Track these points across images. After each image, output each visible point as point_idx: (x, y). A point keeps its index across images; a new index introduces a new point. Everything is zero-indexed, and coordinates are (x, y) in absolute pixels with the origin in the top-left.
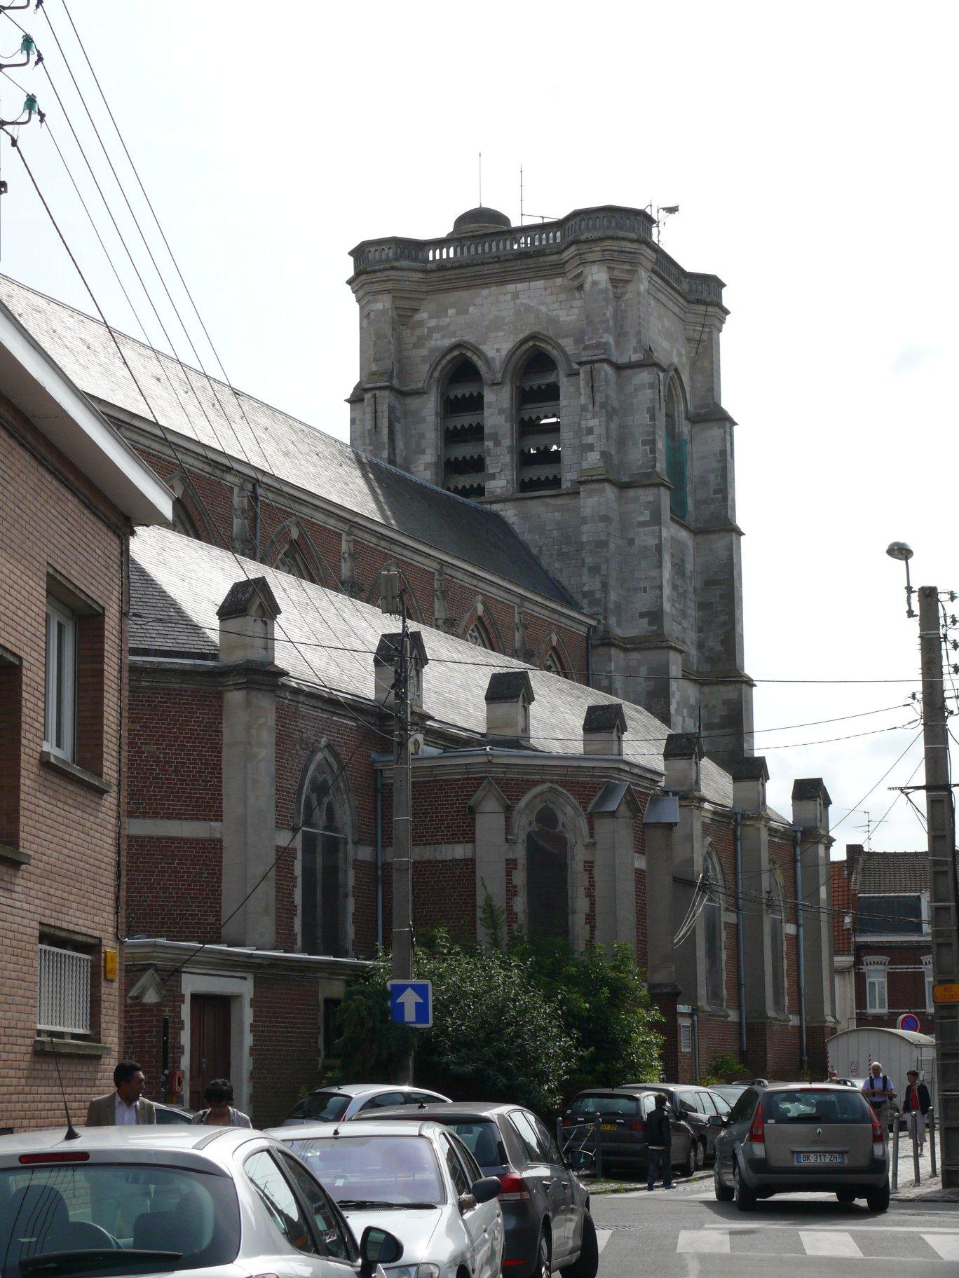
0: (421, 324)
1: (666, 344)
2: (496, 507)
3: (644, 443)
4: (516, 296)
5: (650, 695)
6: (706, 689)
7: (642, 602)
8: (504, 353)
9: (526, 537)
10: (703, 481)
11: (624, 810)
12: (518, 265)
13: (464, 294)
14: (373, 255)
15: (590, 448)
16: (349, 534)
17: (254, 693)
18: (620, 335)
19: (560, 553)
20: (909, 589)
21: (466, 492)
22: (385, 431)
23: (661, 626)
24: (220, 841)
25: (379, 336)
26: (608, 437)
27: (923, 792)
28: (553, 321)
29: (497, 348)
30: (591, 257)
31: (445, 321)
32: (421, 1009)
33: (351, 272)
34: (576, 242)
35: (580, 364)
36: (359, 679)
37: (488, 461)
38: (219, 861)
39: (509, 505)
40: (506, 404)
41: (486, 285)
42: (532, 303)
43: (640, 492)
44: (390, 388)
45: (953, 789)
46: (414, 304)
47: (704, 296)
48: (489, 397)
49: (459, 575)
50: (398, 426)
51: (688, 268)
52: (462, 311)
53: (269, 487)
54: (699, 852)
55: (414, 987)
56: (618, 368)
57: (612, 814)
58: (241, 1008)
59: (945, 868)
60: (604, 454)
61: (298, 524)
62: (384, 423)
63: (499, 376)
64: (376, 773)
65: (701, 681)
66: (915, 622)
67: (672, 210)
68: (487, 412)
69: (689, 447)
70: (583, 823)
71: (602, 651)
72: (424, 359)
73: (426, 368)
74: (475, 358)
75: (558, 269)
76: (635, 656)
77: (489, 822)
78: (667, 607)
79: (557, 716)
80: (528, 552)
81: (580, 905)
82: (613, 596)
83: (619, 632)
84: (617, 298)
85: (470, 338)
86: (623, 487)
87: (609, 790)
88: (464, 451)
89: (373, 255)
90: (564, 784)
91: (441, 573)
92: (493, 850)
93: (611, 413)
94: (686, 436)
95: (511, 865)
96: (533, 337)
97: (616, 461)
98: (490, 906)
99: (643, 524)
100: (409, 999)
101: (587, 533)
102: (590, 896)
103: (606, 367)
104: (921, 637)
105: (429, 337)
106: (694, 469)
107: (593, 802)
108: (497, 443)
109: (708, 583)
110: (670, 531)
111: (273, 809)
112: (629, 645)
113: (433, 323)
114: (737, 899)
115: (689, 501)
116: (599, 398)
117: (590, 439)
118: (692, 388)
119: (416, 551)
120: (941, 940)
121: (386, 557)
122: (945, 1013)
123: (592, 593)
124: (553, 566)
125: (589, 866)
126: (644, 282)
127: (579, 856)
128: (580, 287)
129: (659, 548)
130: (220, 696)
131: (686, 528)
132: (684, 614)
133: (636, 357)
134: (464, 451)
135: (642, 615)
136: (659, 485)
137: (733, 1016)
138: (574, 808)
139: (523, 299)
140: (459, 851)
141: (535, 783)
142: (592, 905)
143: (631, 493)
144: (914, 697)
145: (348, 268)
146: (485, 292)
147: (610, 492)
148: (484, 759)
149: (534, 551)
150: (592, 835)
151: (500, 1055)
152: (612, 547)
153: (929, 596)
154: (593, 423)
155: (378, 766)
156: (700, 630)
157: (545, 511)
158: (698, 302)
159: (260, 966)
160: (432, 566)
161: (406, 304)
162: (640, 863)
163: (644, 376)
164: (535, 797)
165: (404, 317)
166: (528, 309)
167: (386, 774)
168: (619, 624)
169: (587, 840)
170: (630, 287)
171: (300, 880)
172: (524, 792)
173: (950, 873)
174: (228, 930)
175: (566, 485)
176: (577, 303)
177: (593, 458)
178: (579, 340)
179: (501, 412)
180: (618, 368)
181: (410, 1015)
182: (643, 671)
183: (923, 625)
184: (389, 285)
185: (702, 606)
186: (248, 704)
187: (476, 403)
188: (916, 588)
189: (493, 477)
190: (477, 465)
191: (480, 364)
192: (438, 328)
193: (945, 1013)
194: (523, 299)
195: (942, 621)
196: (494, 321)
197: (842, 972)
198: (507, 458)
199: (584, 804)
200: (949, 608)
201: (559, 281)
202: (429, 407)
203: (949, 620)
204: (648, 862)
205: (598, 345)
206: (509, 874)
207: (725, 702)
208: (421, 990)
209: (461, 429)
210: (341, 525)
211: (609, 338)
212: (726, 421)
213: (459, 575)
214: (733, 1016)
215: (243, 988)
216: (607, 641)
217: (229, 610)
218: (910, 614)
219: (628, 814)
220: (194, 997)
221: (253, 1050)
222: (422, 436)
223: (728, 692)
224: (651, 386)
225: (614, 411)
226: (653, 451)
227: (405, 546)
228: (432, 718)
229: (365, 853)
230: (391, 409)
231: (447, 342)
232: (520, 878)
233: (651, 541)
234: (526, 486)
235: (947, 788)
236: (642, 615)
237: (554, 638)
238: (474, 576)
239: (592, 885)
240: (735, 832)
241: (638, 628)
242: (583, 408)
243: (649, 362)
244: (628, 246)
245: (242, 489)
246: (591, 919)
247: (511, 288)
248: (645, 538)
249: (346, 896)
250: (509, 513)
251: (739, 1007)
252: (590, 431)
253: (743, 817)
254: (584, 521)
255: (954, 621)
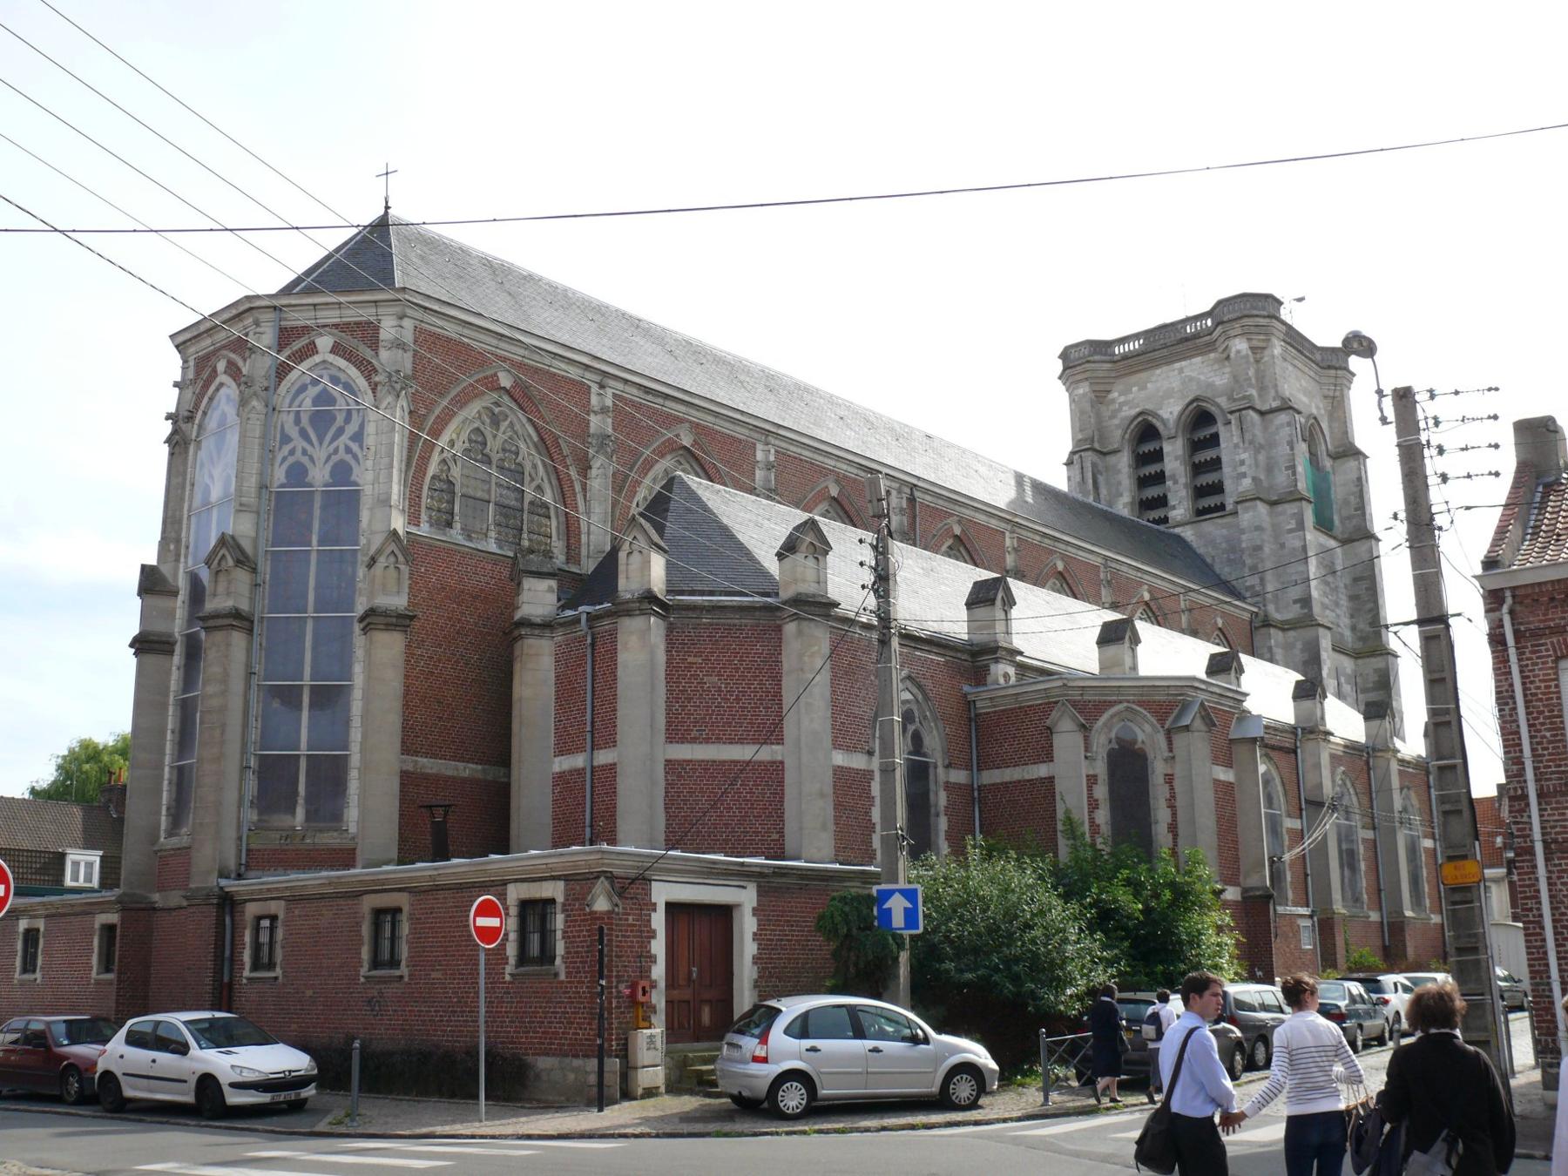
0: (1113, 401)
1: (1305, 399)
2: (1177, 530)
3: (1287, 468)
4: (1181, 370)
5: (1305, 663)
6: (1360, 662)
7: (1295, 593)
8: (1176, 414)
9: (1201, 551)
10: (1346, 502)
11: (1198, 724)
12: (1180, 347)
13: (1144, 375)
14: (1074, 355)
15: (1244, 475)
16: (1012, 532)
17: (805, 623)
18: (1262, 389)
19: (1229, 560)
20: (1380, 393)
21: (1155, 522)
22: (1090, 481)
23: (1311, 608)
24: (782, 763)
25: (1082, 412)
26: (1257, 465)
27: (1415, 628)
28: (1210, 385)
29: (1170, 411)
30: (1232, 333)
31: (1131, 397)
32: (910, 916)
33: (1060, 368)
34: (1222, 323)
35: (1231, 412)
36: (954, 622)
37: (1170, 496)
38: (781, 783)
39: (1188, 527)
40: (1180, 452)
41: (1158, 366)
42: (1194, 374)
43: (1286, 506)
44: (1092, 449)
45: (1451, 621)
46: (1107, 387)
47: (1334, 363)
48: (1167, 448)
49: (1124, 568)
50: (1101, 479)
51: (1319, 343)
52: (1143, 388)
53: (926, 491)
54: (1329, 782)
55: (903, 892)
56: (1262, 413)
57: (1187, 728)
58: (742, 916)
59: (1447, 718)
60: (1254, 479)
61: (959, 522)
62: (1089, 475)
63: (1173, 432)
64: (969, 704)
65: (1356, 655)
66: (1392, 428)
67: (1300, 300)
68: (1166, 460)
69: (1332, 477)
70: (1161, 739)
71: (1264, 630)
72: (1118, 426)
73: (1119, 432)
74: (1154, 421)
75: (1210, 347)
76: (1292, 633)
77: (1067, 741)
78: (1315, 594)
79: (1168, 654)
80: (1203, 561)
81: (1162, 815)
82: (1270, 588)
83: (1277, 616)
84: (1257, 361)
85: (1149, 406)
86: (1273, 504)
87: (1185, 707)
88: (1152, 492)
89: (1074, 355)
90: (1140, 704)
91: (1106, 566)
92: (1074, 771)
93: (1258, 449)
94: (1329, 468)
95: (1092, 780)
96: (1196, 399)
97: (1265, 484)
98: (1069, 819)
99: (1291, 531)
100: (897, 905)
101: (1246, 541)
102: (1172, 807)
103: (1251, 412)
104: (1398, 445)
105: (1120, 410)
106: (1339, 492)
107: (1171, 719)
108: (1176, 482)
109: (1356, 580)
110: (1313, 537)
111: (829, 730)
112: (1285, 627)
113: (1122, 399)
114: (1373, 818)
115: (1336, 518)
116: (1248, 436)
117: (1243, 469)
118: (1331, 433)
119: (1080, 548)
120: (1447, 807)
121: (1051, 552)
122: (1457, 897)
123: (1253, 587)
124: (1225, 571)
125: (1169, 779)
126: (1277, 348)
127: (1158, 769)
128: (1228, 358)
129: (1304, 548)
130: (779, 629)
131: (1335, 538)
132: (1337, 604)
133: (1275, 404)
134: (1152, 492)
135: (1295, 602)
136: (1302, 499)
137: (1374, 916)
138: (1152, 725)
139: (1187, 372)
140: (1042, 771)
141: (1112, 704)
142: (1174, 815)
143: (1280, 508)
144: (1395, 517)
145: (1058, 366)
146: (1158, 371)
147: (1262, 508)
148: (1059, 683)
149: (1209, 560)
150: (1171, 750)
151: (1009, 962)
152: (1267, 550)
153: (1404, 398)
154: (1244, 456)
155: (971, 698)
156: (1352, 616)
157: (1214, 528)
158: (1329, 367)
159: (761, 875)
160: (1098, 561)
161: (1101, 388)
162: (1224, 775)
163: (1283, 418)
164: (1112, 717)
165: (1100, 397)
166: (1191, 379)
167: (979, 704)
168: (1277, 610)
169: (1166, 754)
170: (1267, 352)
171: (877, 801)
172: (1102, 713)
173: (1454, 723)
174: (790, 844)
175: (1229, 507)
176: (1227, 370)
177: (1247, 483)
178: (1231, 399)
179: (1176, 458)
180: (1262, 413)
181: (898, 920)
182: (1299, 645)
183: (1400, 433)
184: (1088, 374)
185: (1353, 598)
186: (800, 633)
187: (1158, 456)
188: (1387, 391)
189: (1174, 508)
190: (1162, 502)
191: (1158, 424)
192: (1125, 403)
193: (1457, 897)
194: (1187, 372)
195: (1422, 425)
196: (1166, 393)
197: (1496, 881)
198: (1183, 493)
199: (1162, 721)
200: (1425, 409)
201: (1212, 355)
202: (1124, 461)
203: (1431, 422)
204: (1236, 775)
205: (1244, 398)
206: (1090, 789)
207: (1375, 671)
208: (910, 895)
209: (1149, 477)
210: (1003, 525)
211: (1254, 392)
212: (1358, 454)
213: (1124, 568)
214: (1374, 916)
215: (745, 898)
216: (1267, 623)
217: (789, 549)
218: (1384, 420)
219: (1203, 728)
220: (671, 907)
221: (756, 960)
222: (1119, 483)
223: (1377, 663)
224: (1289, 424)
225: (1261, 446)
226: (1294, 473)
227: (1068, 543)
228: (1021, 653)
229: (959, 776)
230: (1094, 465)
231: (1134, 412)
232: (1101, 792)
233: (1298, 544)
234: (1200, 512)
235: (1443, 619)
236: (1295, 602)
237: (1220, 622)
238: (1139, 569)
239: (1173, 796)
240: (1367, 763)
241: (1293, 612)
242: (1236, 446)
243: (1286, 407)
244: (1262, 321)
245: (899, 491)
246: (1173, 828)
247: (1177, 365)
248: (1293, 542)
249: (937, 815)
250: (1188, 533)
251: (1381, 909)
252: (1242, 463)
253: (1374, 750)
254: (1243, 532)
255: (1437, 423)
